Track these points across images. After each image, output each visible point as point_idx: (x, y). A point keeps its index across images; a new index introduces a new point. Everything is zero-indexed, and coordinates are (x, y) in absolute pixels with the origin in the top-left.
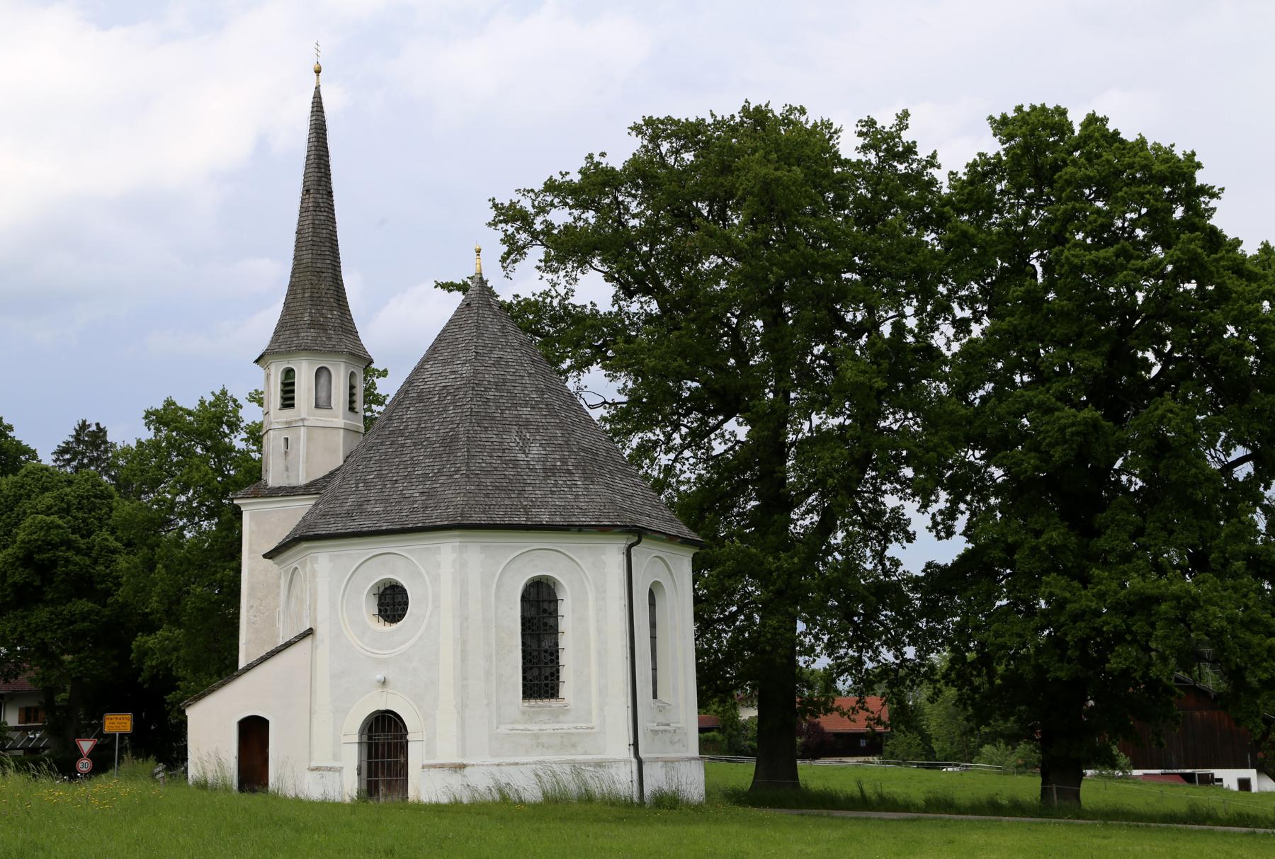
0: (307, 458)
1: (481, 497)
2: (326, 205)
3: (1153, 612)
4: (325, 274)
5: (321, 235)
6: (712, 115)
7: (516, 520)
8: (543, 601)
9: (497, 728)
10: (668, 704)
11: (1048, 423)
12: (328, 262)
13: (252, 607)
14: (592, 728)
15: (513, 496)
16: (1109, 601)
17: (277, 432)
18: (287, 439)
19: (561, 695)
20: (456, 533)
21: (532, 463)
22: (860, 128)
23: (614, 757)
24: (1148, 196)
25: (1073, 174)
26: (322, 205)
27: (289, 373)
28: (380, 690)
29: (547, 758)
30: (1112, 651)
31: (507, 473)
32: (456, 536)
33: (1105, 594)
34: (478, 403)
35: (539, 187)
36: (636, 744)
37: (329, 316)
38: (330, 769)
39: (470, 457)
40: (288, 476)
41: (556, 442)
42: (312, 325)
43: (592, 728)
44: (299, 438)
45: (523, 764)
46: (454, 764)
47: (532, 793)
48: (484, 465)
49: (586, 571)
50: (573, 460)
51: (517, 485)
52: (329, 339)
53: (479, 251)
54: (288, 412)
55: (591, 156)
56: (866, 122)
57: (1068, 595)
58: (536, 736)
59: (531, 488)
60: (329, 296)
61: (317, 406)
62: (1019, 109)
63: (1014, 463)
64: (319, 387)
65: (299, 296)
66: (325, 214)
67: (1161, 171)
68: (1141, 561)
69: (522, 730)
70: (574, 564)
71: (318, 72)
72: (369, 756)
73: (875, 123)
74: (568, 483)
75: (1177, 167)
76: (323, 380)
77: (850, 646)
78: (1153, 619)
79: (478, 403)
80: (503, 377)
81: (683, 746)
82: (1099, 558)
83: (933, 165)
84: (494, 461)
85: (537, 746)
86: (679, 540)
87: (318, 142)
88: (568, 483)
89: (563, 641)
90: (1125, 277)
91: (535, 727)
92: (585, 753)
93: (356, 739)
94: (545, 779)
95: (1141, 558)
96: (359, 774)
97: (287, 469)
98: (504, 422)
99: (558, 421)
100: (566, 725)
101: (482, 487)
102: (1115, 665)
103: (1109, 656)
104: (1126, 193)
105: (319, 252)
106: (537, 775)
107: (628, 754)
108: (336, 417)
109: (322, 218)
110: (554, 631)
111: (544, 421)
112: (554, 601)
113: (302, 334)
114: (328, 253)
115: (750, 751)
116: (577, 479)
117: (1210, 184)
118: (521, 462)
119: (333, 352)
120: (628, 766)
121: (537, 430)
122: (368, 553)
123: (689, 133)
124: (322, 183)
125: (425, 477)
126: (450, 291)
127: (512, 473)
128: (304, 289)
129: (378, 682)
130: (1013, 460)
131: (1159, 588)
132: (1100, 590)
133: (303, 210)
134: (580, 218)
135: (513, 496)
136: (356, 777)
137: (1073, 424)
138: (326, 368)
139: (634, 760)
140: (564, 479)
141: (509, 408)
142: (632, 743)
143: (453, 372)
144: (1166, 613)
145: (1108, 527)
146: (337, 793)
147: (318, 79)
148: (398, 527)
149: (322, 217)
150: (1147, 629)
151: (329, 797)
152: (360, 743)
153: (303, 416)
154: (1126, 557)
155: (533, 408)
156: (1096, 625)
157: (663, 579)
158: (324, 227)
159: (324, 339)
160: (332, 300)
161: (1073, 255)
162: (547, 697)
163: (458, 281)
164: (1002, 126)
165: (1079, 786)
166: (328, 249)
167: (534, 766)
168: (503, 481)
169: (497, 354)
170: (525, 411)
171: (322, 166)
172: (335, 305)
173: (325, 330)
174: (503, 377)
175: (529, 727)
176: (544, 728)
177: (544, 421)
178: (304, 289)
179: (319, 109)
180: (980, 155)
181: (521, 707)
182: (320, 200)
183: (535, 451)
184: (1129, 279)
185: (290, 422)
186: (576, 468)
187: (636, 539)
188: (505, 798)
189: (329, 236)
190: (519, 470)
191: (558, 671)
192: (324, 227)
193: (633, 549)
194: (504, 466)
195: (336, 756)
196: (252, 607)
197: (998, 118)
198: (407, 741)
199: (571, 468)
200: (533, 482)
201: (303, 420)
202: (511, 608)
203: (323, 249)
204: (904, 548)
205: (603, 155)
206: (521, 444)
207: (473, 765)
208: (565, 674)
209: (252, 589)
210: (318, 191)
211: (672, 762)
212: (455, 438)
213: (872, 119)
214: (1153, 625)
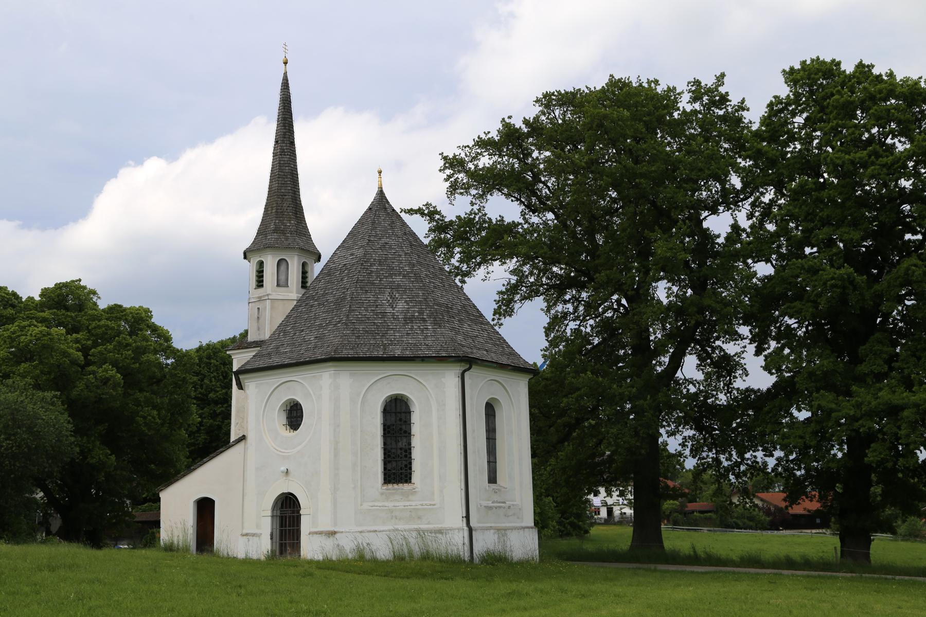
0: (271, 323)
1: (353, 339)
2: (288, 150)
3: (899, 417)
4: (287, 197)
5: (284, 171)
6: (587, 88)
7: (375, 354)
8: (400, 413)
9: (361, 505)
10: (504, 488)
11: (816, 280)
12: (289, 188)
13: (237, 423)
14: (434, 505)
15: (377, 337)
16: (864, 409)
17: (253, 304)
18: (259, 308)
19: (413, 481)
20: (330, 364)
21: (396, 314)
22: (690, 87)
23: (450, 526)
24: (893, 111)
25: (837, 100)
26: (286, 151)
27: (261, 264)
28: (284, 478)
29: (400, 527)
30: (869, 447)
31: (376, 321)
32: (330, 366)
33: (861, 404)
34: (364, 274)
35: (471, 144)
36: (467, 517)
37: (288, 224)
38: (254, 535)
39: (351, 311)
40: (259, 334)
41: (417, 299)
42: (276, 231)
43: (434, 505)
44: (266, 307)
45: (381, 531)
46: (329, 531)
47: (383, 551)
48: (360, 316)
49: (429, 389)
50: (428, 312)
51: (383, 329)
52: (287, 239)
53: (380, 172)
54: (260, 290)
55: (503, 119)
56: (694, 82)
57: (833, 406)
58: (391, 511)
59: (392, 332)
60: (289, 211)
61: (278, 285)
62: (803, 63)
63: (795, 311)
64: (280, 272)
65: (269, 212)
66: (288, 157)
67: (902, 93)
68: (893, 380)
69: (380, 506)
70: (421, 385)
71: (286, 63)
72: (281, 526)
73: (700, 83)
74: (421, 327)
75: (915, 89)
76: (283, 268)
77: (710, 450)
78: (899, 423)
79: (364, 274)
80: (386, 256)
81: (518, 518)
82: (860, 380)
83: (743, 109)
84: (368, 314)
85: (392, 518)
86: (510, 368)
87: (284, 109)
88: (421, 327)
89: (416, 442)
90: (872, 171)
91: (390, 504)
92: (429, 523)
93: (269, 513)
94: (395, 543)
95: (894, 378)
96: (272, 539)
97: (259, 329)
98: (381, 287)
99: (421, 285)
100: (415, 502)
101: (355, 332)
102: (872, 459)
103: (867, 451)
104: (876, 110)
105: (283, 182)
106: (390, 538)
107: (461, 524)
108: (291, 292)
109: (286, 159)
110: (408, 434)
111: (411, 285)
112: (408, 413)
113: (269, 237)
114: (289, 182)
115: (734, 525)
116: (429, 324)
117: (915, 77)
118: (389, 314)
119: (288, 248)
120: (461, 532)
121: (405, 292)
122: (278, 381)
123: (569, 99)
124: (287, 136)
125: (320, 326)
126: (412, 214)
127: (380, 322)
128: (272, 207)
129: (283, 472)
130: (794, 309)
131: (903, 399)
132: (857, 401)
133: (275, 155)
134: (635, 214)
135: (377, 337)
136: (269, 540)
137: (833, 278)
138: (286, 261)
139: (466, 528)
140: (419, 325)
141: (386, 277)
142: (464, 515)
143: (352, 255)
144: (908, 417)
145: (867, 356)
146: (254, 552)
147: (286, 68)
148: (295, 361)
149: (286, 158)
150: (895, 430)
151: (250, 555)
152: (272, 516)
153: (269, 292)
154: (879, 377)
155: (404, 276)
156: (855, 428)
157: (499, 394)
158: (287, 165)
159: (283, 240)
160: (291, 214)
161: (836, 158)
162: (402, 483)
163: (416, 208)
164: (791, 76)
165: (869, 548)
166: (289, 179)
167: (388, 533)
168: (372, 327)
169: (384, 240)
170: (398, 279)
171: (286, 125)
172: (292, 217)
173: (284, 234)
174: (386, 256)
175: (386, 504)
176: (398, 505)
177: (411, 285)
178: (272, 207)
179: (285, 87)
180: (775, 97)
181: (380, 490)
182: (285, 148)
183: (401, 305)
184: (876, 172)
185: (260, 297)
186: (430, 317)
187: (468, 366)
188: (361, 557)
189: (289, 171)
190: (386, 319)
191: (410, 463)
192: (287, 165)
193: (467, 375)
194: (375, 316)
195: (258, 526)
196: (237, 423)
197: (788, 70)
198: (300, 515)
199: (425, 317)
200: (395, 327)
201: (268, 295)
202: (373, 418)
203: (286, 180)
204: (744, 381)
205: (510, 117)
206: (391, 301)
207: (342, 532)
208: (416, 466)
209: (238, 411)
210: (283, 142)
211: (505, 530)
212: (344, 298)
213: (698, 80)
214: (899, 428)
